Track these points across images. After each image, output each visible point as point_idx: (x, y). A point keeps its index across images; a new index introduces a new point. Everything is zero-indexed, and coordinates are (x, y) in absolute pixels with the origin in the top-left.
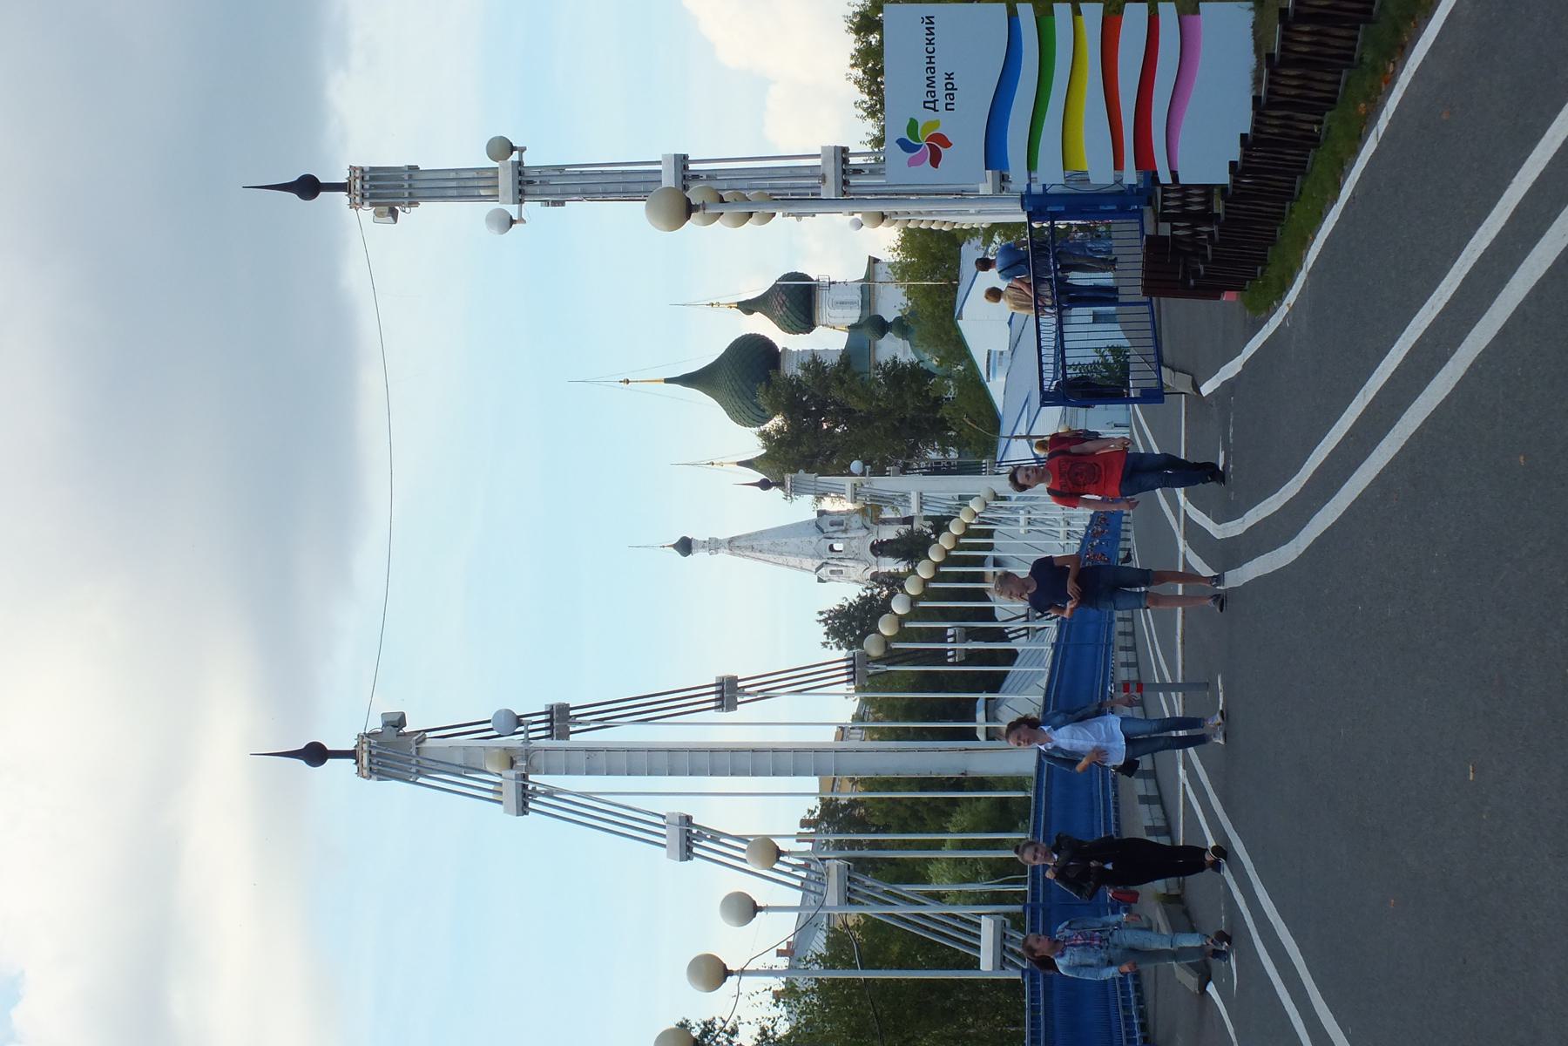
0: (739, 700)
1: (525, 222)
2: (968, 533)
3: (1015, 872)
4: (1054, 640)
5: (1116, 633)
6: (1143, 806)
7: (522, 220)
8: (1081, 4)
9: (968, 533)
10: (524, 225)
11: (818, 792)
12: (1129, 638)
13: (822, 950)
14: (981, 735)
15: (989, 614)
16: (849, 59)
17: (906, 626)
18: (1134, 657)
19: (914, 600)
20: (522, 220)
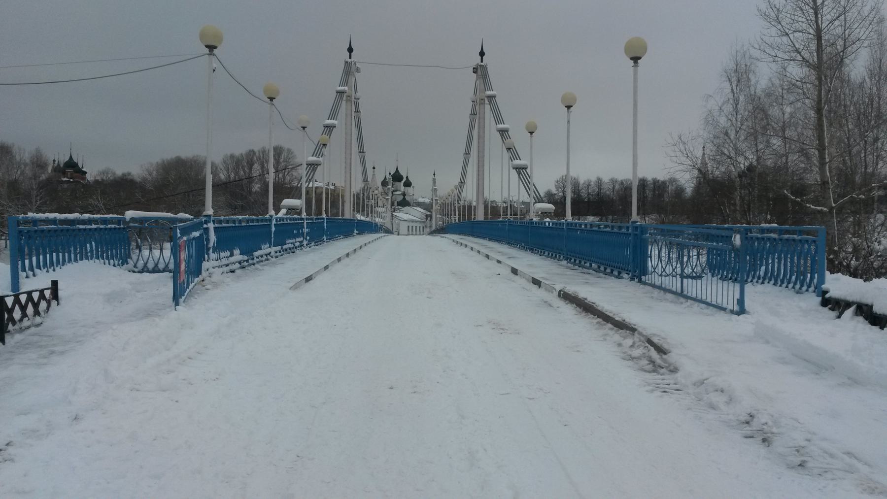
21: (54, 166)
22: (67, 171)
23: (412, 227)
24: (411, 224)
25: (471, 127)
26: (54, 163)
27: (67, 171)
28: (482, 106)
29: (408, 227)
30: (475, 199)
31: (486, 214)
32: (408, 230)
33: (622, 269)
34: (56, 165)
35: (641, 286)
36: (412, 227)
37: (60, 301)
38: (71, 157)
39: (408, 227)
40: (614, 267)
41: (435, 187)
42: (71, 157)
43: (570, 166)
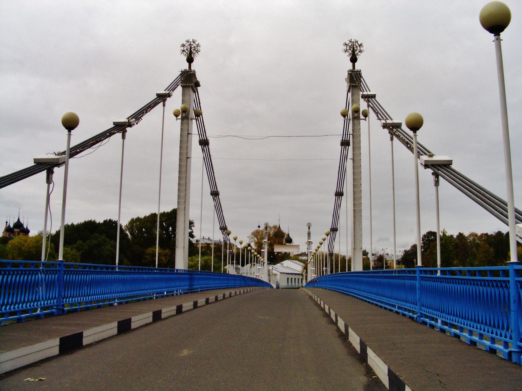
0: (222, 231)
1: (176, 120)
2: (257, 258)
3: (476, 263)
4: (246, 276)
5: (236, 291)
6: (152, 313)
7: (177, 119)
8: (46, 170)
9: (257, 258)
10: (176, 120)
11: (214, 240)
12: (239, 293)
13: (211, 246)
14: (511, 273)
15: (247, 263)
16: (185, 40)
17: (249, 252)
18: (189, 308)
19: (253, 253)
20: (177, 119)
21: (6, 226)
22: (15, 230)
23: (292, 279)
24: (290, 277)
25: (343, 158)
26: (7, 224)
27: (15, 230)
28: (356, 121)
29: (288, 279)
30: (294, 244)
31: (15, 231)
32: (288, 282)
33: (438, 316)
34: (8, 225)
35: (166, 321)
36: (292, 279)
37: (337, 334)
38: (19, 219)
39: (288, 279)
40: (438, 316)
41: (310, 241)
42: (19, 219)
43: (91, 137)
